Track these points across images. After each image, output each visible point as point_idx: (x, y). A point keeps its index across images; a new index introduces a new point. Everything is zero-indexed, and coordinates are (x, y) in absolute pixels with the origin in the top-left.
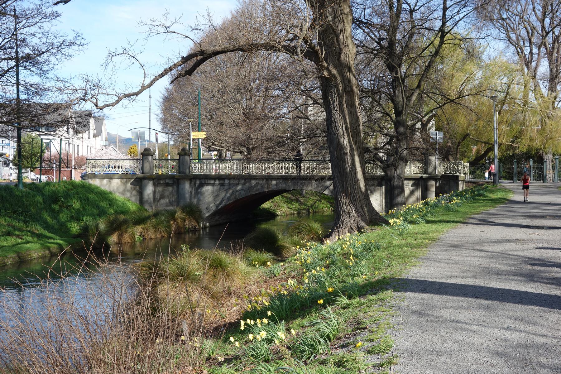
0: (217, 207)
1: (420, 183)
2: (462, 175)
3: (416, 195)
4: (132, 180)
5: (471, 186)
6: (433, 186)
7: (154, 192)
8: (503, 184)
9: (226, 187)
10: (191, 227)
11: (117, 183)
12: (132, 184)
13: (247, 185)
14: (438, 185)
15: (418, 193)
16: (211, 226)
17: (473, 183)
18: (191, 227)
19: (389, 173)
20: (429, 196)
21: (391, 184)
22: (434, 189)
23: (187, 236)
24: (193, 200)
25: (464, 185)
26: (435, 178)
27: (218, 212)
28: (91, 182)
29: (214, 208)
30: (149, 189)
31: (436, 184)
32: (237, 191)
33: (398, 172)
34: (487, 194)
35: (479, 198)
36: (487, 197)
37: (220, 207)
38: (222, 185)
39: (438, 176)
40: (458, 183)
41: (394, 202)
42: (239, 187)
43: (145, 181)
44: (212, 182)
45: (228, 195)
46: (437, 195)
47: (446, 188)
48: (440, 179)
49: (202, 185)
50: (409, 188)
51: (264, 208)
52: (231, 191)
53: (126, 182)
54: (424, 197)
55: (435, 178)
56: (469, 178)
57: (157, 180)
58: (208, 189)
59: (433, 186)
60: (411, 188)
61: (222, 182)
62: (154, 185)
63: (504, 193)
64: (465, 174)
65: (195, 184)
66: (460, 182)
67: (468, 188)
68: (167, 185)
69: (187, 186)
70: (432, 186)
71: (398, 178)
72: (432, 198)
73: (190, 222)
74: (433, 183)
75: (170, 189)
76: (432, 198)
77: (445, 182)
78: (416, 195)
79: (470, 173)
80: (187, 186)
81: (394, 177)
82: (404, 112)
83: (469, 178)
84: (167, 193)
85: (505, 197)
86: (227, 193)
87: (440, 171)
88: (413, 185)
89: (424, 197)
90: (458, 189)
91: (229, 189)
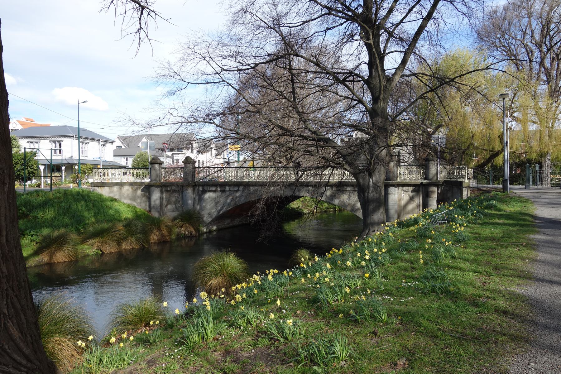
0: (219, 212)
1: (421, 189)
2: (467, 180)
3: (416, 202)
4: (142, 187)
5: (477, 193)
6: (435, 193)
7: (161, 199)
8: (515, 191)
9: (228, 193)
10: (187, 233)
11: (128, 190)
12: (142, 191)
13: (246, 191)
14: (439, 191)
15: (419, 200)
16: (218, 230)
17: (479, 189)
18: (187, 233)
19: (361, 181)
20: (430, 203)
21: (364, 195)
22: (435, 196)
23: (183, 242)
24: (196, 205)
25: (469, 192)
26: (437, 184)
27: (219, 218)
28: (99, 190)
29: (215, 214)
30: (156, 195)
31: (438, 190)
32: (237, 197)
33: (374, 179)
34: (499, 206)
35: (490, 212)
36: (500, 210)
37: (221, 212)
38: (223, 191)
39: (439, 182)
40: (462, 190)
41: (369, 221)
42: (238, 194)
43: (152, 188)
44: (214, 189)
45: (228, 201)
46: (438, 202)
47: (449, 195)
48: (442, 185)
49: (204, 192)
50: (409, 195)
51: (293, 209)
52: (231, 197)
53: (137, 189)
54: (425, 205)
55: (437, 184)
56: (473, 183)
57: (165, 187)
58: (209, 195)
59: (435, 193)
60: (411, 194)
61: (223, 189)
62: (162, 192)
63: (522, 205)
64: (469, 179)
65: (198, 190)
66: (464, 189)
67: (474, 195)
68: (174, 191)
69: (190, 193)
70: (433, 192)
71: (374, 188)
72: (433, 203)
73: (186, 228)
74: (435, 189)
75: (176, 195)
76: (433, 203)
77: (447, 188)
78: (416, 202)
79: (474, 177)
80: (190, 193)
81: (368, 186)
82: (382, 97)
83: (473, 183)
84: (173, 199)
85: (525, 210)
86: (227, 199)
87: (442, 176)
88: (413, 191)
89: (425, 205)
90: (462, 197)
91: (230, 195)
